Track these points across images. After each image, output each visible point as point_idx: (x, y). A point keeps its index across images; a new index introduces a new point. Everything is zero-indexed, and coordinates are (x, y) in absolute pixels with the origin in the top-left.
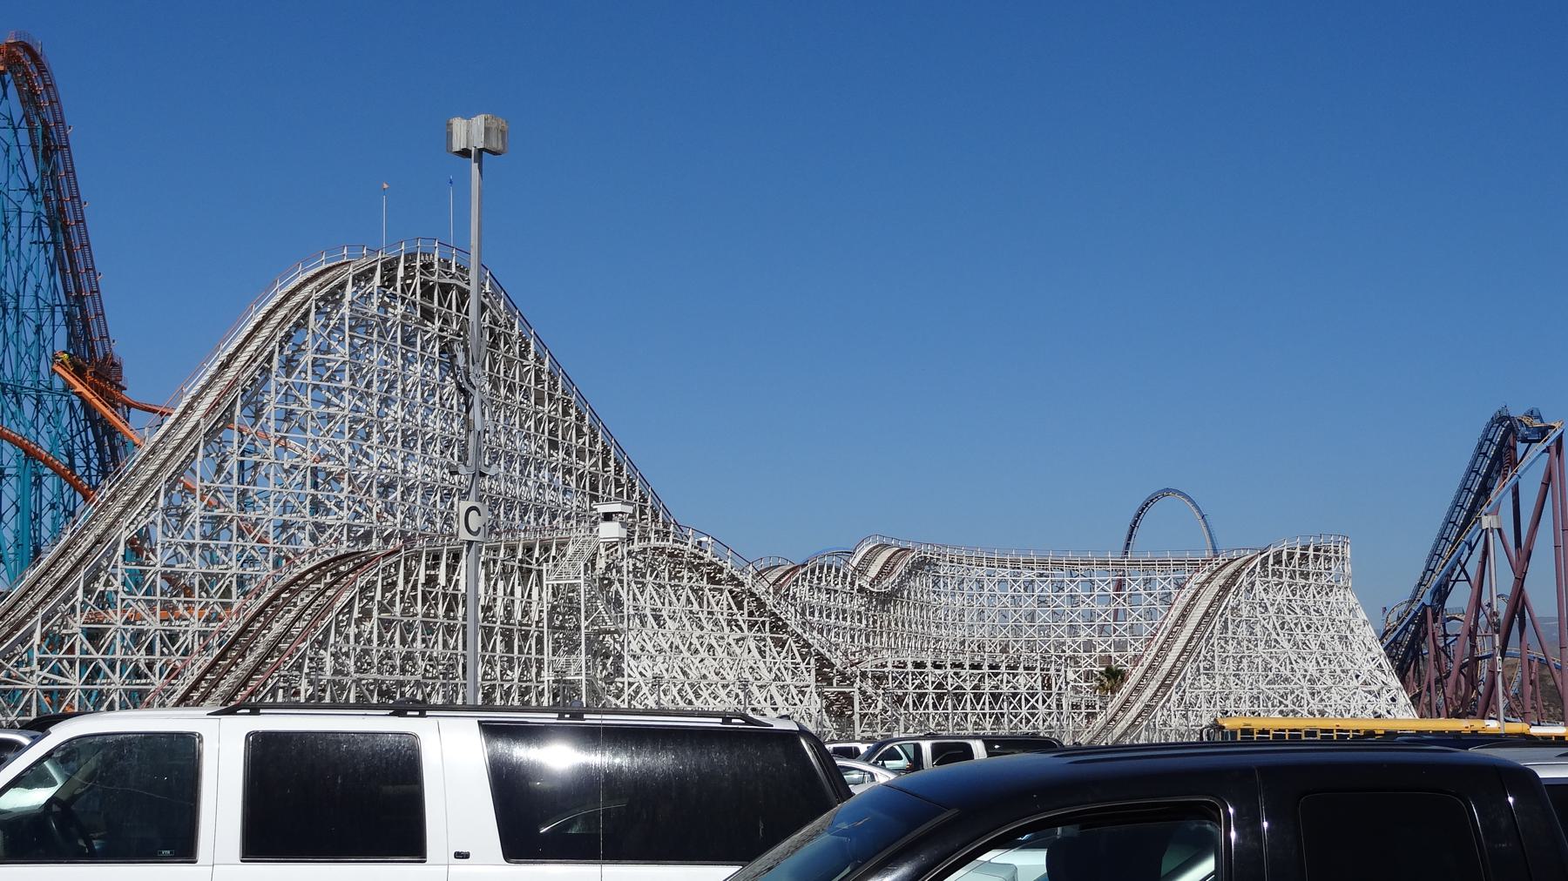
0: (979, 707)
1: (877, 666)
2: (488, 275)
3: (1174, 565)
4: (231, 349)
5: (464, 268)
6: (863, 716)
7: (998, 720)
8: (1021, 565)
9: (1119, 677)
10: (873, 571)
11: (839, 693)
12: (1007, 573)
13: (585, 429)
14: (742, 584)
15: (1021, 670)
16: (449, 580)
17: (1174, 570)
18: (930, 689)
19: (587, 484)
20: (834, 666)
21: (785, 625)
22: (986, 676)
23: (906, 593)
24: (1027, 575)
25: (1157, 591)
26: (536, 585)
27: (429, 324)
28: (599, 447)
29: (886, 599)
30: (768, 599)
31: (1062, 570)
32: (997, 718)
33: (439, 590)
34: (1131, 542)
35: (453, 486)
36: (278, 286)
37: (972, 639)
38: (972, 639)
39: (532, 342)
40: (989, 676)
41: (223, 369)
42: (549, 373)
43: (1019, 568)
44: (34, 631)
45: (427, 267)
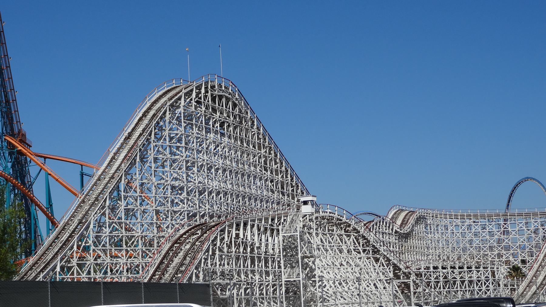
0: (463, 287)
1: (417, 269)
2: (237, 90)
3: (540, 215)
4: (129, 130)
5: (227, 87)
6: (415, 293)
7: (472, 292)
8: (465, 217)
9: (519, 271)
10: (399, 222)
11: (402, 282)
12: (458, 221)
13: (278, 161)
14: (359, 232)
15: (481, 269)
16: (244, 235)
17: (540, 218)
18: (441, 279)
19: (280, 186)
20: (401, 269)
21: (379, 251)
22: (466, 272)
23: (414, 233)
24: (468, 222)
25: (532, 228)
26: (276, 236)
27: (214, 114)
28: (283, 168)
29: (406, 236)
30: (371, 239)
31: (485, 219)
32: (472, 292)
33: (240, 240)
34: (510, 204)
35: (227, 190)
36: (147, 99)
37: (444, 254)
38: (444, 254)
39: (255, 120)
40: (467, 272)
41: (127, 140)
42: (263, 135)
43: (464, 219)
44: (57, 266)
45: (213, 87)
